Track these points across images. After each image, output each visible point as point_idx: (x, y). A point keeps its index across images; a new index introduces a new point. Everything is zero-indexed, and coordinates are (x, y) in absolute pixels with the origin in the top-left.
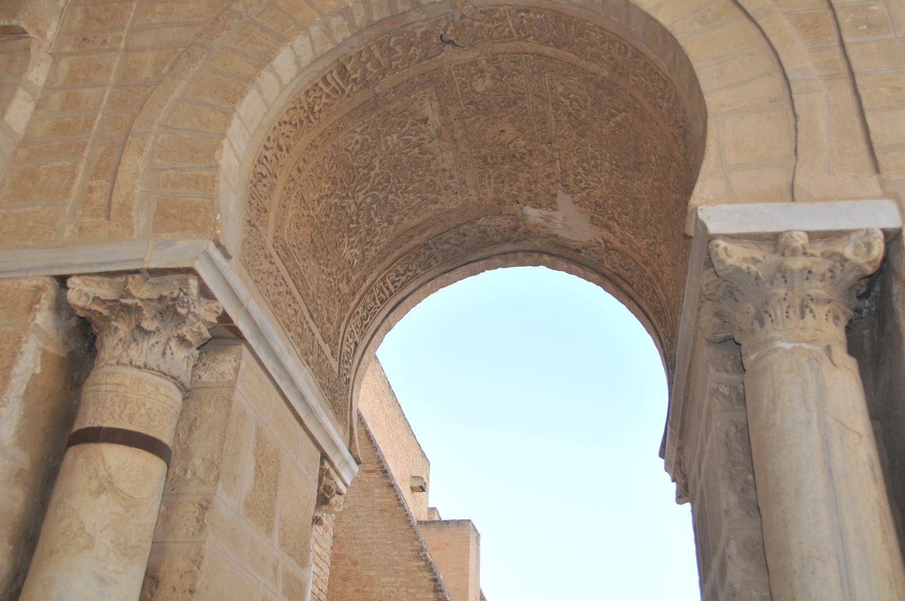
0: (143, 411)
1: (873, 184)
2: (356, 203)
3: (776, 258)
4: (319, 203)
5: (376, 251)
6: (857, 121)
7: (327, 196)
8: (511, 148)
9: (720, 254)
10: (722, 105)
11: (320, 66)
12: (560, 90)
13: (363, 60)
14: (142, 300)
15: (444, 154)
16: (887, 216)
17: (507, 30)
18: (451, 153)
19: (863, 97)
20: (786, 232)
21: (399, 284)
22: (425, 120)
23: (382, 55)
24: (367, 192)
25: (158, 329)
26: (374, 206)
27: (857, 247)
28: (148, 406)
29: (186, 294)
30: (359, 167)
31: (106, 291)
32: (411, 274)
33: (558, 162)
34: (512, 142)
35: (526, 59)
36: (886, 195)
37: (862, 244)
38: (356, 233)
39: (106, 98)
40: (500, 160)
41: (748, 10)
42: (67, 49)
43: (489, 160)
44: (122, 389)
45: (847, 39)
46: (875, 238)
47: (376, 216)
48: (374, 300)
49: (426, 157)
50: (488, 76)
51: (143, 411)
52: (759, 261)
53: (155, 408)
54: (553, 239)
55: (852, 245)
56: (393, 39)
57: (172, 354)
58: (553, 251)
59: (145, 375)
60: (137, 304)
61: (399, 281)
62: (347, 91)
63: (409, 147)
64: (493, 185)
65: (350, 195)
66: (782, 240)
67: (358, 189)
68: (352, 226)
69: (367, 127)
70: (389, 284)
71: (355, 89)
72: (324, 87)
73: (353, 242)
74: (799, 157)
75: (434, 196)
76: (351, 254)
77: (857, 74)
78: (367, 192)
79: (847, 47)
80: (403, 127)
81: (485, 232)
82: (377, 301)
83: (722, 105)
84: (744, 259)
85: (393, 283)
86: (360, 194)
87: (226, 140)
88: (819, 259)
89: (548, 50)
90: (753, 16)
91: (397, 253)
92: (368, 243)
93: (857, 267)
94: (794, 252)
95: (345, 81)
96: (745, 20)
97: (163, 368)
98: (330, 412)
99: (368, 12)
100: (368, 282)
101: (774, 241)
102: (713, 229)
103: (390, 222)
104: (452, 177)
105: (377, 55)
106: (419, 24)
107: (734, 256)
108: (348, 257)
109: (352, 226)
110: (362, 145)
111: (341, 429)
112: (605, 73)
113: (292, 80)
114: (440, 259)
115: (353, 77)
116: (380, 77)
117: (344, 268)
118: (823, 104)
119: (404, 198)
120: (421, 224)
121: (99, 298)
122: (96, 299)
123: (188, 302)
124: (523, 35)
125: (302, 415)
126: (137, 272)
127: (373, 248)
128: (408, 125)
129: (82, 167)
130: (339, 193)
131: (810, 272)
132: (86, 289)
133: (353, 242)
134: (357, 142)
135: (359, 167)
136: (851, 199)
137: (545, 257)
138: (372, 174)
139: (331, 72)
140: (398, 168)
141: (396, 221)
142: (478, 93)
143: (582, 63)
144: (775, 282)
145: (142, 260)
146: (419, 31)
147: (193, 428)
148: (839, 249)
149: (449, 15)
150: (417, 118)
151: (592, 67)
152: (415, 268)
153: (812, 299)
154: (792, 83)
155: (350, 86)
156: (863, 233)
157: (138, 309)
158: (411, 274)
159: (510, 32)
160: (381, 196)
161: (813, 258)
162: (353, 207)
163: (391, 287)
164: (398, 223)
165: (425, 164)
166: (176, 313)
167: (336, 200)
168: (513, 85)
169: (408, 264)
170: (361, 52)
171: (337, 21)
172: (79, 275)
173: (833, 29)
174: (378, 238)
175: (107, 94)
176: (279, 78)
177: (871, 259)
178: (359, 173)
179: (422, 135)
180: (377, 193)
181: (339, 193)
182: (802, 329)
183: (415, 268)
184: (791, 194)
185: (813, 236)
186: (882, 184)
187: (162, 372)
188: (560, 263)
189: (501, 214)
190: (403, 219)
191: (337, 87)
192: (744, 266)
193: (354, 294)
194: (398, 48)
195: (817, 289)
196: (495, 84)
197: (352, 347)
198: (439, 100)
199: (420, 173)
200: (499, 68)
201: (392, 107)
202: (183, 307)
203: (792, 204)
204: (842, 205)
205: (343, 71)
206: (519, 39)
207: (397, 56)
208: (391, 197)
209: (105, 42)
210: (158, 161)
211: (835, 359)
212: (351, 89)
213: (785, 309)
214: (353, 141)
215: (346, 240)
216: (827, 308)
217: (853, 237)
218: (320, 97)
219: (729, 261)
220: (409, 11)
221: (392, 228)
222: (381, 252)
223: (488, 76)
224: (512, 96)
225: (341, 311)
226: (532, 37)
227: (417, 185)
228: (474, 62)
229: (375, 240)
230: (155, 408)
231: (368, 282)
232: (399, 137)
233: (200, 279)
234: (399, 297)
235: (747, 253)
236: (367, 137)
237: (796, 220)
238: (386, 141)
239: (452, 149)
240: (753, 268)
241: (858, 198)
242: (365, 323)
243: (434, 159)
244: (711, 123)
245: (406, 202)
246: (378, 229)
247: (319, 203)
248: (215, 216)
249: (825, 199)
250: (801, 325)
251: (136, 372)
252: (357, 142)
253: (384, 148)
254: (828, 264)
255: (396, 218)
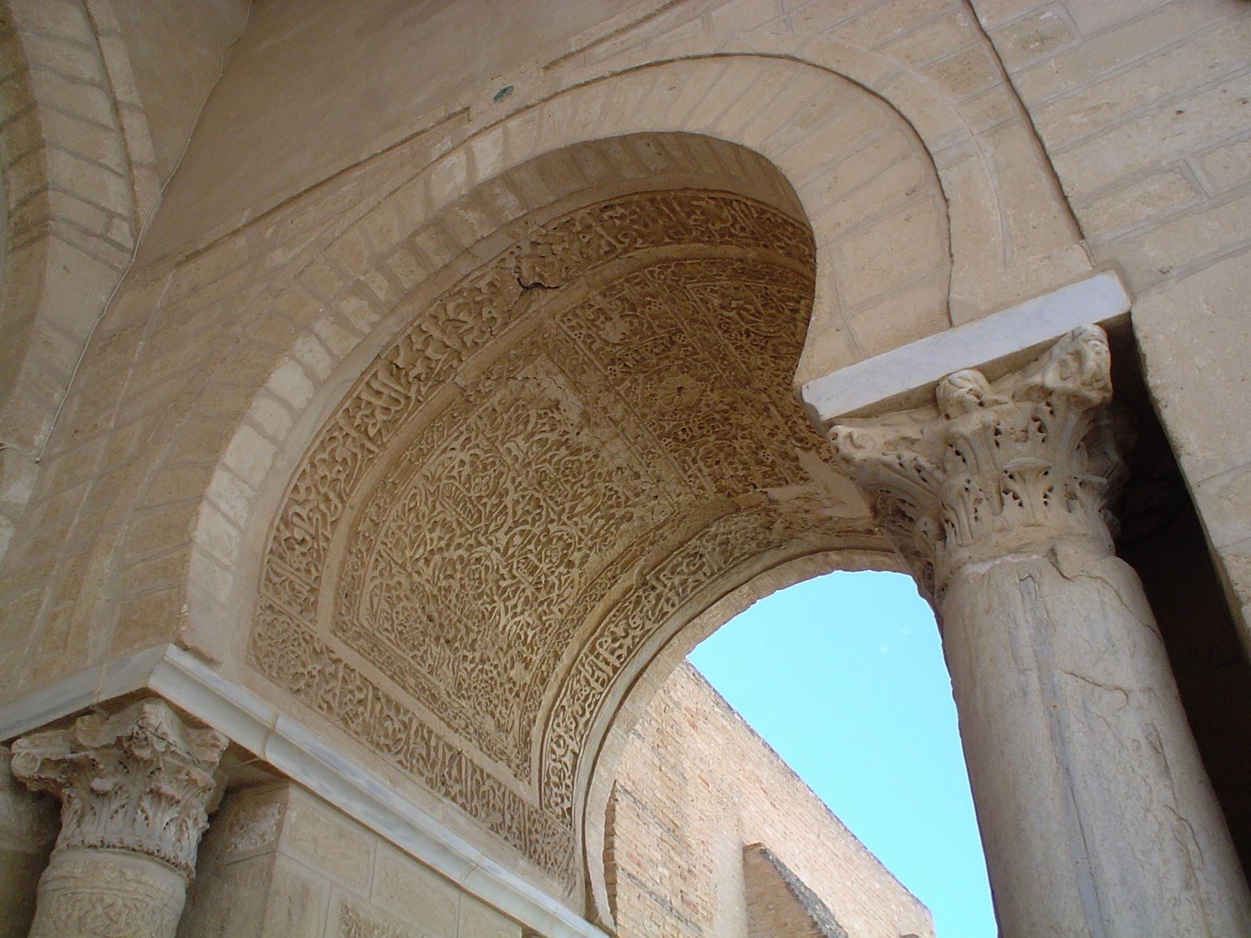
0: (100, 910)
1: (1076, 257)
2: (498, 550)
3: (942, 423)
4: (427, 561)
5: (561, 611)
6: (1044, 175)
7: (441, 549)
8: (705, 409)
9: (841, 447)
10: (838, 225)
11: (354, 371)
12: (717, 302)
13: (418, 346)
14: (97, 749)
15: (608, 446)
16: (1102, 300)
17: (603, 242)
18: (619, 442)
19: (1044, 138)
20: (943, 379)
21: (624, 652)
22: (556, 405)
23: (443, 332)
24: (510, 529)
25: (119, 788)
26: (531, 547)
27: (1063, 364)
28: (108, 901)
29: (141, 728)
30: (481, 497)
31: (56, 747)
32: (638, 632)
33: (772, 408)
34: (699, 401)
35: (652, 273)
36: (1099, 268)
37: (1068, 357)
38: (515, 592)
39: (86, 494)
40: (697, 432)
41: (866, 84)
42: (57, 450)
43: (682, 436)
44: (71, 883)
45: (1012, 69)
46: (1086, 341)
47: (540, 560)
48: (588, 683)
49: (582, 458)
50: (616, 316)
51: (100, 910)
52: (913, 442)
53: (120, 902)
54: (828, 524)
55: (1055, 364)
56: (451, 307)
57: (146, 818)
58: (839, 542)
59: (103, 856)
60: (87, 756)
61: (621, 647)
62: (412, 394)
63: (550, 449)
64: (706, 471)
65: (483, 540)
66: (940, 393)
67: (492, 528)
68: (503, 584)
69: (468, 439)
70: (606, 655)
71: (424, 390)
72: (373, 400)
73: (515, 606)
74: (955, 259)
75: (623, 511)
76: (517, 624)
77: (1031, 110)
78: (510, 529)
79: (1013, 79)
80: (527, 423)
81: (727, 542)
82: (593, 684)
83: (838, 225)
84: (888, 444)
85: (612, 653)
86: (500, 534)
87: (205, 502)
88: (1011, 405)
89: (671, 251)
90: (873, 89)
91: (600, 607)
92: (541, 603)
93: (1073, 399)
94: (963, 407)
95: (403, 381)
96: (866, 99)
97: (130, 841)
98: (523, 863)
99: (393, 280)
100: (566, 659)
101: (931, 399)
102: (826, 411)
103: (570, 564)
104: (637, 476)
105: (437, 334)
106: (477, 274)
107: (869, 444)
108: (512, 628)
109: (503, 584)
110: (473, 464)
111: (557, 886)
112: (752, 254)
113: (309, 401)
114: (676, 599)
115: (413, 373)
116: (455, 363)
117: (509, 647)
118: (987, 174)
119: (576, 524)
120: (621, 555)
121: (49, 760)
122: (46, 762)
123: (146, 738)
124: (627, 241)
125: (455, 875)
126: (87, 712)
127: (555, 609)
128: (533, 420)
129: (49, 590)
130: (462, 540)
131: (997, 432)
132: (35, 751)
133: (515, 606)
134: (462, 463)
135: (481, 497)
136: (1044, 292)
137: (834, 556)
138: (508, 501)
139: (375, 375)
140: (546, 483)
141: (577, 562)
142: (614, 345)
143: (720, 251)
144: (948, 467)
145: (91, 693)
146: (482, 284)
147: (225, 925)
148: (1037, 379)
149: (514, 249)
150: (542, 404)
151: (733, 251)
152: (639, 622)
153: (1011, 477)
154: (935, 157)
155: (414, 388)
156: (1067, 339)
157: (93, 764)
158: (638, 632)
159: (610, 244)
160: (537, 530)
161: (996, 408)
162: (495, 556)
163: (613, 660)
164: (582, 564)
165: (585, 467)
166: (138, 760)
167: (460, 552)
168: (654, 317)
169: (627, 617)
170: (409, 337)
171: (350, 306)
172: (28, 734)
173: (993, 62)
174: (557, 592)
175: (88, 489)
176: (284, 402)
177: (1087, 376)
178: (485, 505)
179: (561, 428)
180: (527, 527)
181: (462, 540)
182: (1000, 531)
183: (639, 622)
184: (948, 318)
185: (992, 372)
186: (1090, 256)
187: (127, 848)
188: (858, 557)
189: (738, 509)
190: (588, 556)
191: (393, 395)
192: (891, 458)
193: (544, 681)
194: (462, 317)
195: (1020, 455)
196: (631, 324)
197: (568, 759)
198: (562, 371)
199: (586, 482)
200: (622, 300)
201: (495, 400)
202: (142, 747)
203: (949, 332)
204: (1030, 307)
205: (395, 371)
206: (626, 250)
207: (466, 327)
208: (553, 528)
209: (95, 426)
210: (128, 555)
211: (1064, 566)
212: (419, 391)
213: (970, 506)
214: (456, 463)
215: (500, 605)
216: (1043, 486)
217: (1056, 350)
218: (373, 414)
219: (858, 455)
220: (451, 262)
221: (575, 572)
222: (572, 610)
223: (616, 316)
224: (661, 332)
225: (525, 710)
226: (640, 241)
227: (589, 500)
228: (586, 304)
229: (554, 595)
230: (120, 902)
231: (566, 659)
232: (527, 439)
233: (168, 702)
234: (632, 670)
235: (891, 435)
236: (477, 451)
237: (955, 358)
238: (509, 450)
239: (617, 435)
240: (908, 456)
241: (1053, 289)
242: (582, 721)
243: (596, 456)
244: (821, 256)
245: (582, 530)
246: (552, 579)
247: (427, 561)
248: (180, 606)
249: (1000, 307)
250: (998, 525)
251: (91, 854)
252: (462, 463)
253: (509, 461)
254: (1028, 406)
255: (576, 557)
